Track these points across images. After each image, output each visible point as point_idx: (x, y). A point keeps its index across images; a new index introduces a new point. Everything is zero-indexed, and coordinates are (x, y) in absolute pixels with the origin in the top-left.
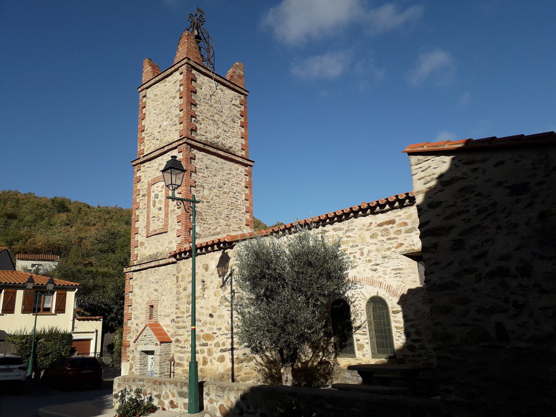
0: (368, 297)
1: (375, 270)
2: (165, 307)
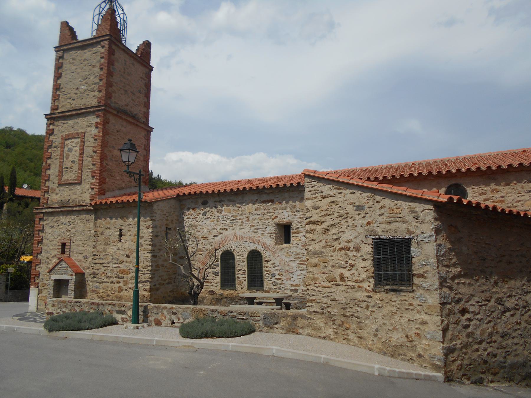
0: (249, 249)
1: (256, 232)
2: (78, 245)
